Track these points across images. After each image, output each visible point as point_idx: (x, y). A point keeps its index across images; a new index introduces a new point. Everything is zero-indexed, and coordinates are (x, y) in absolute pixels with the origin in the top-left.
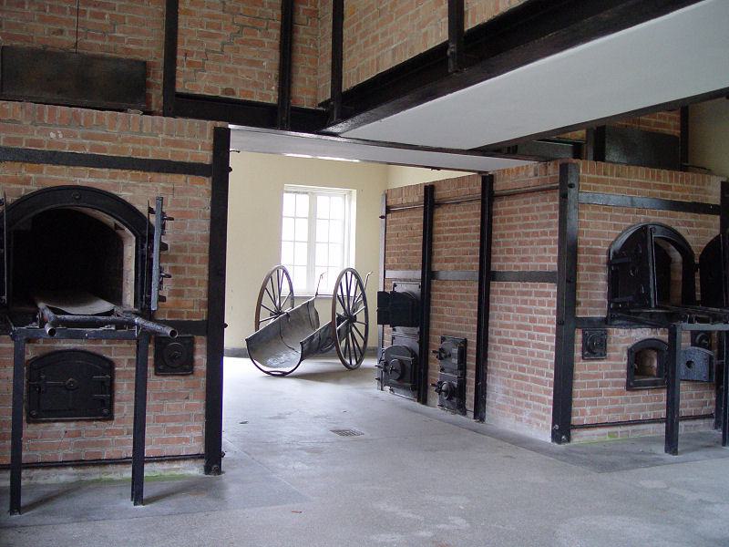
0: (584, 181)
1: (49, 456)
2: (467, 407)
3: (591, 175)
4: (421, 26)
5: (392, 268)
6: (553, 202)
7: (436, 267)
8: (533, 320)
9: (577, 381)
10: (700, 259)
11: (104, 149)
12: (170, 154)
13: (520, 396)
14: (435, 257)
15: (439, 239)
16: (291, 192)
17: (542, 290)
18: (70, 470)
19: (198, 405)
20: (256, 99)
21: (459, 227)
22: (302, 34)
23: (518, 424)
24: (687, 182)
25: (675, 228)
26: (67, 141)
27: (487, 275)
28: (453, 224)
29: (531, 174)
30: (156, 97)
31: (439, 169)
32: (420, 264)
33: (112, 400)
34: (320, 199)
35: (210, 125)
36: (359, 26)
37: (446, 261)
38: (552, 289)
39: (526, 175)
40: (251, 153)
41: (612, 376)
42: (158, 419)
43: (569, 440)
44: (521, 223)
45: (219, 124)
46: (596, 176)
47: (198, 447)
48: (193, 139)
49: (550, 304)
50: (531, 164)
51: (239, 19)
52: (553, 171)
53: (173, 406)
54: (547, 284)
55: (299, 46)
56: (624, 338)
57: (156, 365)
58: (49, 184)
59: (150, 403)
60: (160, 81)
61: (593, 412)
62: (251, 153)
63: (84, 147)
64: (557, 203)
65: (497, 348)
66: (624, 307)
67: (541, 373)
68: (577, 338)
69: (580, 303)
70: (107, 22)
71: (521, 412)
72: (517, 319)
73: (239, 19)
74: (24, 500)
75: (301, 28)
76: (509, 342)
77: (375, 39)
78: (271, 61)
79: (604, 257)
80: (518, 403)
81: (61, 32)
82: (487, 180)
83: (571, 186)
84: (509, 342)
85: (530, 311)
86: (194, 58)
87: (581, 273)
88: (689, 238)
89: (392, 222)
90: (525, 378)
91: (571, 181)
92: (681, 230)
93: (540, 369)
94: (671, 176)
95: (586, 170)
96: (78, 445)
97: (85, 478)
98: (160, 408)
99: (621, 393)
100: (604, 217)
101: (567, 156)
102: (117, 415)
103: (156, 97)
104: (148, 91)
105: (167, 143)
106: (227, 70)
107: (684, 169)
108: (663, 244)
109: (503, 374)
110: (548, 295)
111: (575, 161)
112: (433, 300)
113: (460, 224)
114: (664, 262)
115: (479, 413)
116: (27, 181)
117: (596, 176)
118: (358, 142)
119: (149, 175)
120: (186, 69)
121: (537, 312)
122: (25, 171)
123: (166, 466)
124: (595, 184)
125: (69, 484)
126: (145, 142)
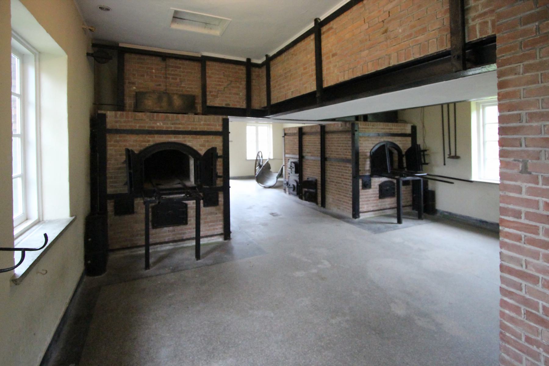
1: (162, 240)
4: (303, 84)
5: (288, 154)
6: (349, 136)
7: (304, 154)
8: (342, 175)
9: (361, 197)
11: (180, 128)
12: (206, 128)
18: (171, 244)
19: (220, 216)
20: (238, 107)
21: (312, 144)
22: (254, 83)
23: (339, 210)
26: (165, 126)
27: (324, 159)
30: (199, 108)
33: (187, 217)
35: (221, 117)
36: (277, 82)
37: (308, 153)
38: (350, 166)
40: (234, 123)
42: (205, 223)
43: (359, 217)
45: (224, 117)
47: (221, 231)
48: (214, 122)
49: (349, 170)
51: (230, 79)
53: (211, 219)
55: (253, 88)
56: (377, 181)
57: (530, 187)
58: (158, 142)
59: (202, 217)
60: (200, 101)
61: (367, 207)
62: (234, 123)
63: (171, 128)
66: (377, 171)
70: (178, 80)
73: (230, 79)
74: (152, 260)
75: (254, 81)
77: (284, 87)
78: (243, 93)
79: (368, 154)
81: (160, 85)
83: (356, 131)
86: (214, 93)
87: (360, 160)
88: (400, 146)
91: (356, 129)
92: (397, 143)
96: (174, 235)
97: (177, 247)
98: (206, 218)
99: (377, 200)
100: (368, 141)
102: (189, 223)
103: (199, 108)
104: (196, 105)
105: (204, 125)
106: (227, 97)
107: (397, 122)
108: (391, 148)
110: (348, 167)
111: (357, 122)
114: (391, 153)
115: (323, 204)
116: (149, 141)
119: (198, 137)
120: (211, 97)
122: (148, 138)
123: (209, 238)
125: (172, 249)
126: (196, 124)
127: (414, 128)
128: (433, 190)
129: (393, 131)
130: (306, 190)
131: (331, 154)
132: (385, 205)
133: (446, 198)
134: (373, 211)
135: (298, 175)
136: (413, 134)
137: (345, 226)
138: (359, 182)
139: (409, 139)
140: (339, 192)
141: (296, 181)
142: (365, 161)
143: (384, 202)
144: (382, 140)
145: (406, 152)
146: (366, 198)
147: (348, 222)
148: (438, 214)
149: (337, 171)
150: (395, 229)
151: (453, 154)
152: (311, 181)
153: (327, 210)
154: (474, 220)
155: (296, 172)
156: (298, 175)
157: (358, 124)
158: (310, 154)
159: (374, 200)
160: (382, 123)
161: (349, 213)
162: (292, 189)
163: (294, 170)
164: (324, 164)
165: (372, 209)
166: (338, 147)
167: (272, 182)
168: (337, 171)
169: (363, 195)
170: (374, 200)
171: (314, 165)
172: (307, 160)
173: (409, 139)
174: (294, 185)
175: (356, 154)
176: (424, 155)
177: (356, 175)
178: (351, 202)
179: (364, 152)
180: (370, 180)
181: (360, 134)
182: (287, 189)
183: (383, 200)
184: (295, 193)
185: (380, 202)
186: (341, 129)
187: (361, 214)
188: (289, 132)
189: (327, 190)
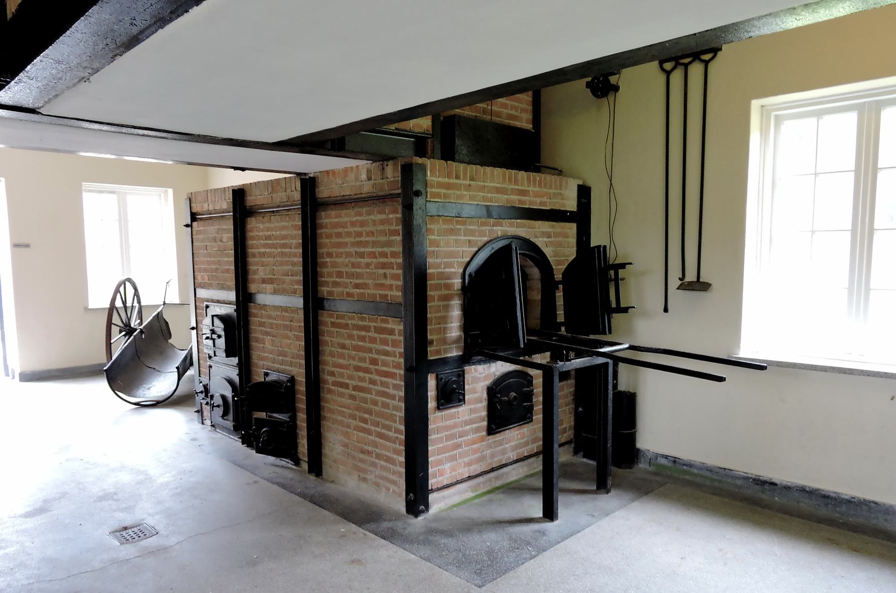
0: (432, 187)
2: (300, 456)
3: (440, 179)
5: (204, 286)
6: (393, 215)
7: (253, 288)
8: (374, 362)
9: (432, 437)
10: (563, 274)
13: (363, 452)
14: (251, 277)
15: (254, 256)
16: (93, 191)
17: (384, 325)
21: (277, 241)
23: (364, 485)
24: (545, 187)
25: (532, 240)
27: (314, 303)
28: (268, 238)
29: (364, 176)
31: (243, 169)
32: (232, 283)
34: (130, 199)
37: (264, 281)
39: (357, 179)
41: (472, 422)
44: (352, 240)
46: (446, 180)
49: (395, 344)
50: (362, 164)
52: (392, 172)
54: (390, 319)
56: (481, 376)
61: (453, 469)
64: (400, 216)
65: (330, 391)
66: (477, 347)
67: (389, 428)
68: (426, 382)
69: (432, 342)
71: (365, 471)
72: (354, 359)
76: (346, 386)
79: (457, 282)
80: (361, 461)
82: (308, 184)
83: (418, 194)
84: (346, 386)
85: (370, 350)
88: (548, 251)
89: (199, 232)
90: (369, 432)
91: (417, 187)
92: (540, 242)
93: (387, 423)
94: (529, 180)
95: (435, 173)
99: (482, 439)
100: (452, 232)
101: (407, 154)
107: (538, 170)
109: (341, 423)
110: (391, 332)
111: (420, 160)
112: (252, 327)
113: (276, 238)
115: (316, 467)
117: (446, 180)
118: (170, 135)
121: (378, 352)
124: (445, 191)
127: (584, 192)
128: (632, 391)
129: (535, 202)
130: (263, 415)
131: (336, 284)
132: (504, 452)
133: (670, 418)
134: (470, 478)
135: (235, 360)
136: (581, 217)
137: (384, 555)
138: (426, 382)
139: (571, 229)
140: (365, 421)
141: (230, 382)
142: (447, 308)
143: (501, 443)
144: (499, 231)
145: (566, 273)
146: (448, 438)
147: (390, 536)
148: (642, 465)
149: (356, 348)
150: (542, 550)
151: (691, 277)
152: (276, 384)
153: (329, 489)
154: (739, 478)
155: (229, 353)
156: (235, 360)
157: (423, 168)
158: (269, 287)
159: (474, 442)
160: (498, 171)
161: (394, 498)
162: (219, 411)
163: (221, 342)
164: (316, 323)
165: (465, 472)
166: (362, 253)
167: (163, 384)
168: (356, 348)
169: (438, 430)
170: (474, 442)
171: (286, 327)
172: (264, 307)
173: (571, 229)
174: (224, 397)
175: (418, 280)
176: (617, 280)
177: (418, 362)
178: (402, 459)
179: (442, 276)
180: (461, 375)
181: (432, 209)
182: (207, 409)
183: (498, 437)
184: (230, 424)
185: (489, 446)
186: (367, 188)
187: (432, 497)
188: (205, 207)
189: (326, 414)
